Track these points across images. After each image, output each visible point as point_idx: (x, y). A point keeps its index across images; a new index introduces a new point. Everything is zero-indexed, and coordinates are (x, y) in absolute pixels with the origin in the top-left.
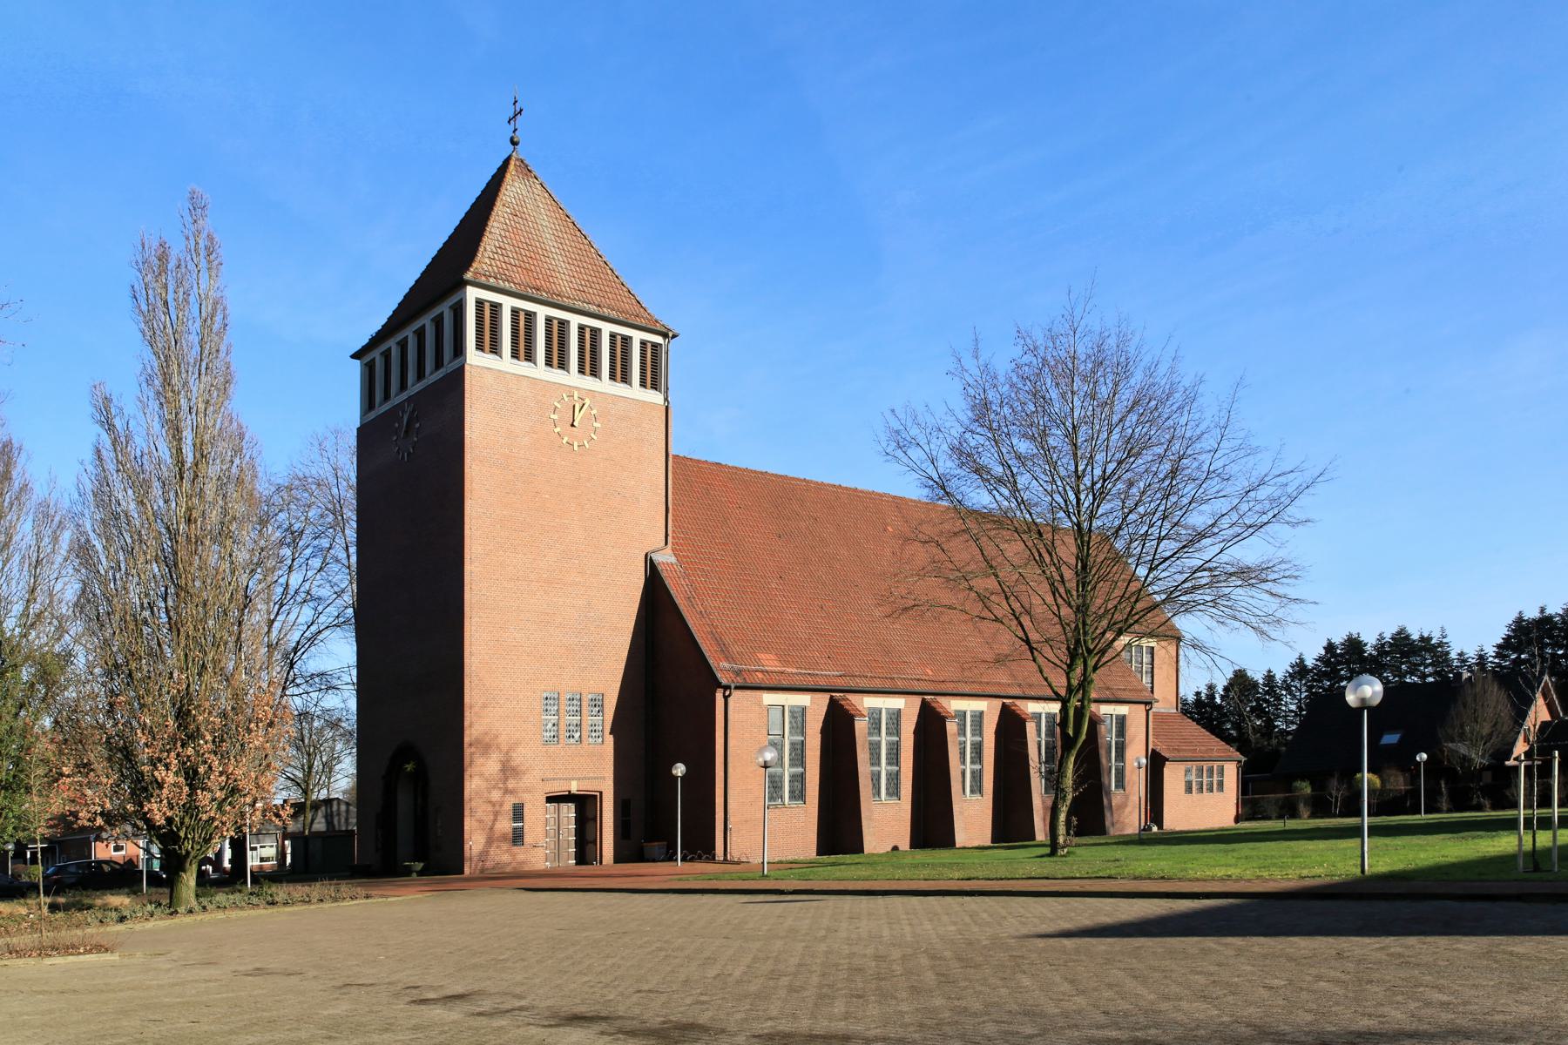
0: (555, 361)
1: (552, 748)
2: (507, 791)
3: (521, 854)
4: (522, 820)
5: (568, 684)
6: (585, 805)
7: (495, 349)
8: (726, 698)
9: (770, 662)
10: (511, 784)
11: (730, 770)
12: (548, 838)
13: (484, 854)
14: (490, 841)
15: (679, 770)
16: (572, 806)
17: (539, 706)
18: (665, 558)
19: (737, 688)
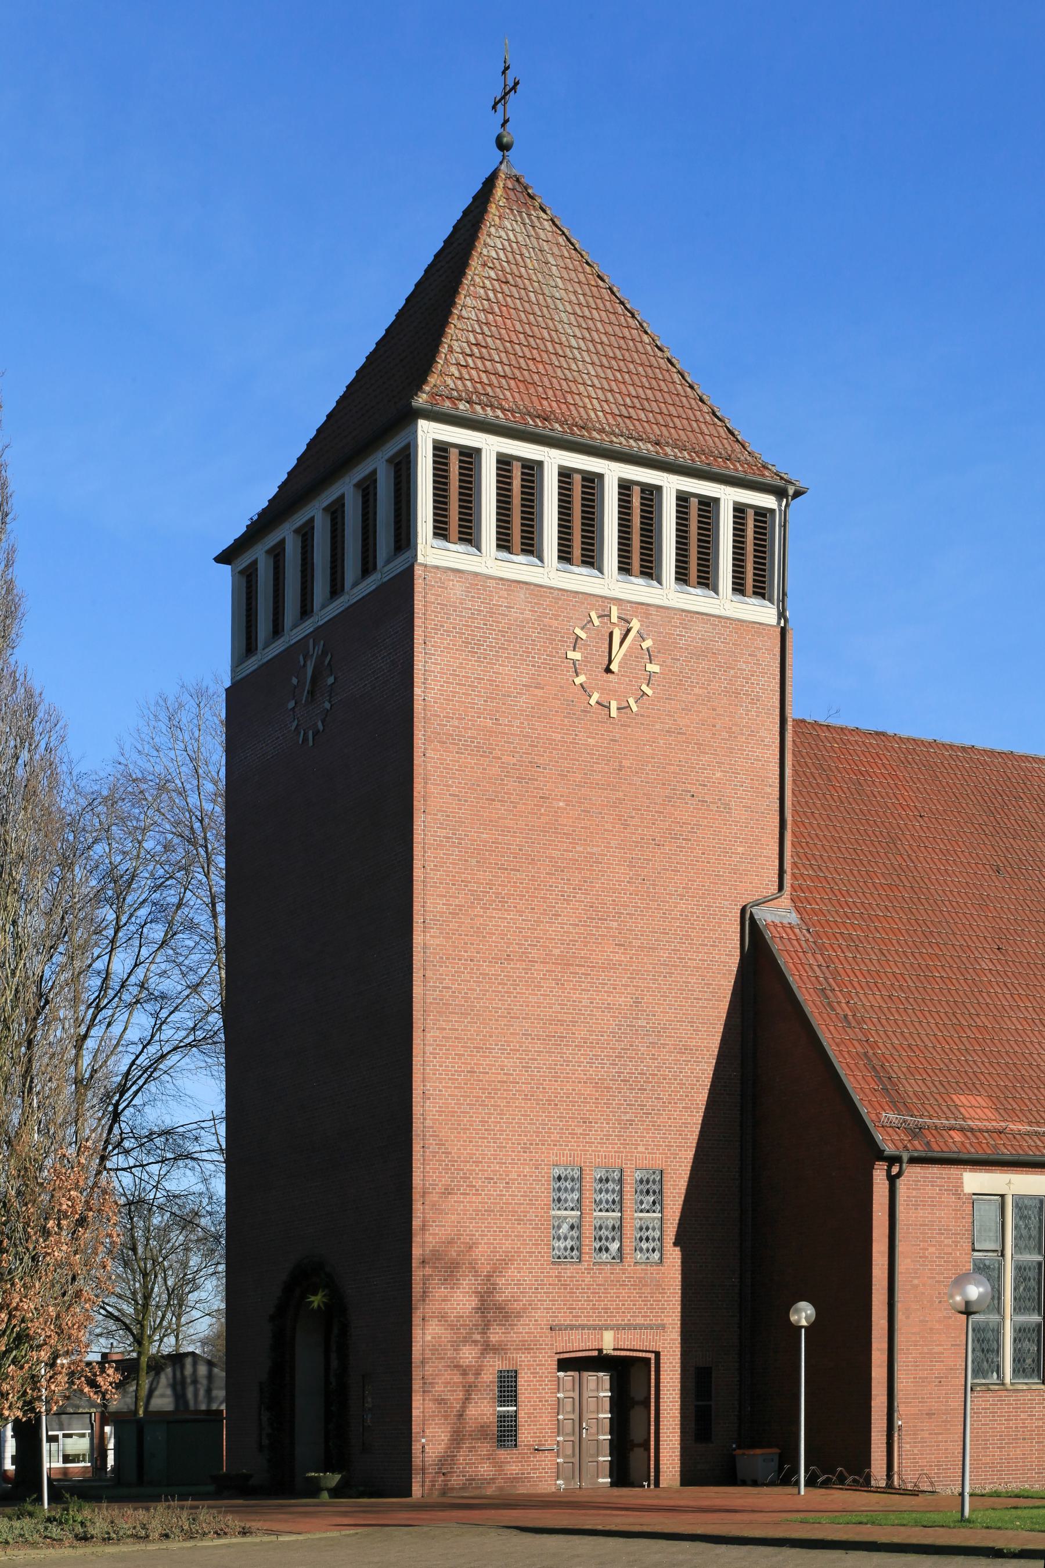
1: (569, 1271)
2: (488, 1348)
5: (597, 1153)
6: (628, 1374)
7: (469, 536)
8: (892, 1180)
9: (977, 1111)
10: (496, 1335)
11: (899, 1307)
12: (559, 1436)
13: (446, 1463)
14: (457, 1438)
15: (803, 1314)
16: (605, 1377)
17: (544, 1192)
18: (778, 915)
19: (913, 1161)
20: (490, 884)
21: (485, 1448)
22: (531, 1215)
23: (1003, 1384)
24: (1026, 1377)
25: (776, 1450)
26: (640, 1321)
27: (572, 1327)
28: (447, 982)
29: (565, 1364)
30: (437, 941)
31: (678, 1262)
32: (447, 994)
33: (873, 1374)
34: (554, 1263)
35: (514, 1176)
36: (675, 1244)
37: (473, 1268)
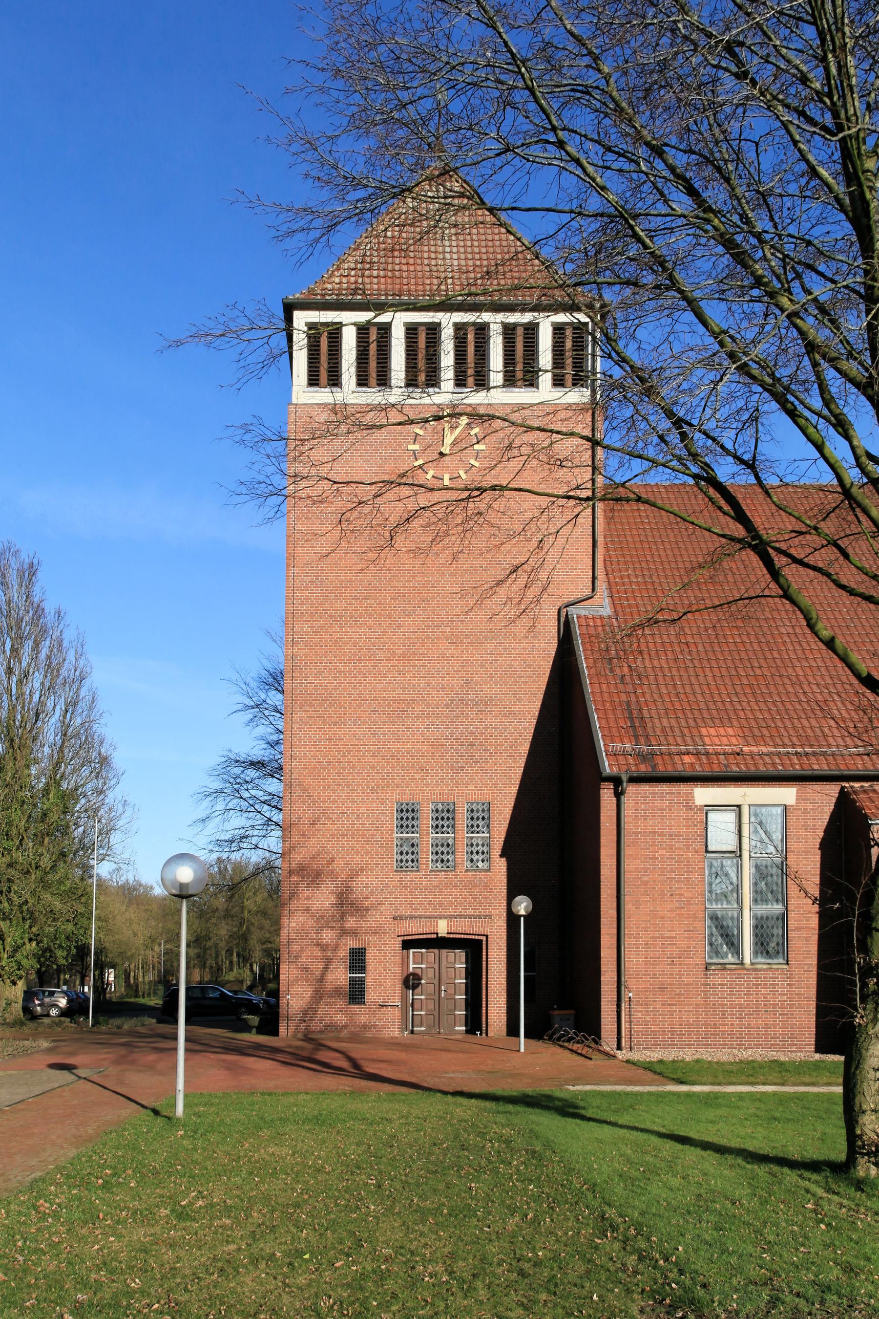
0: (373, 380)
2: (344, 932)
3: (362, 1015)
4: (363, 969)
5: (428, 796)
8: (618, 795)
9: (721, 740)
10: (351, 922)
11: (627, 899)
13: (308, 1013)
14: (319, 995)
19: (633, 780)
20: (346, 610)
21: (341, 1003)
22: (378, 837)
23: (742, 964)
24: (771, 957)
25: (573, 1012)
26: (470, 912)
27: (411, 917)
28: (311, 679)
29: (407, 945)
30: (304, 652)
31: (504, 869)
32: (311, 688)
33: (602, 955)
34: (396, 871)
35: (363, 810)
36: (501, 856)
37: (334, 876)
